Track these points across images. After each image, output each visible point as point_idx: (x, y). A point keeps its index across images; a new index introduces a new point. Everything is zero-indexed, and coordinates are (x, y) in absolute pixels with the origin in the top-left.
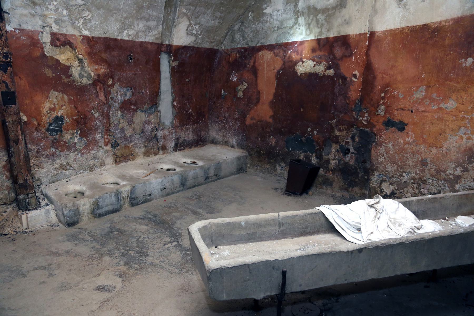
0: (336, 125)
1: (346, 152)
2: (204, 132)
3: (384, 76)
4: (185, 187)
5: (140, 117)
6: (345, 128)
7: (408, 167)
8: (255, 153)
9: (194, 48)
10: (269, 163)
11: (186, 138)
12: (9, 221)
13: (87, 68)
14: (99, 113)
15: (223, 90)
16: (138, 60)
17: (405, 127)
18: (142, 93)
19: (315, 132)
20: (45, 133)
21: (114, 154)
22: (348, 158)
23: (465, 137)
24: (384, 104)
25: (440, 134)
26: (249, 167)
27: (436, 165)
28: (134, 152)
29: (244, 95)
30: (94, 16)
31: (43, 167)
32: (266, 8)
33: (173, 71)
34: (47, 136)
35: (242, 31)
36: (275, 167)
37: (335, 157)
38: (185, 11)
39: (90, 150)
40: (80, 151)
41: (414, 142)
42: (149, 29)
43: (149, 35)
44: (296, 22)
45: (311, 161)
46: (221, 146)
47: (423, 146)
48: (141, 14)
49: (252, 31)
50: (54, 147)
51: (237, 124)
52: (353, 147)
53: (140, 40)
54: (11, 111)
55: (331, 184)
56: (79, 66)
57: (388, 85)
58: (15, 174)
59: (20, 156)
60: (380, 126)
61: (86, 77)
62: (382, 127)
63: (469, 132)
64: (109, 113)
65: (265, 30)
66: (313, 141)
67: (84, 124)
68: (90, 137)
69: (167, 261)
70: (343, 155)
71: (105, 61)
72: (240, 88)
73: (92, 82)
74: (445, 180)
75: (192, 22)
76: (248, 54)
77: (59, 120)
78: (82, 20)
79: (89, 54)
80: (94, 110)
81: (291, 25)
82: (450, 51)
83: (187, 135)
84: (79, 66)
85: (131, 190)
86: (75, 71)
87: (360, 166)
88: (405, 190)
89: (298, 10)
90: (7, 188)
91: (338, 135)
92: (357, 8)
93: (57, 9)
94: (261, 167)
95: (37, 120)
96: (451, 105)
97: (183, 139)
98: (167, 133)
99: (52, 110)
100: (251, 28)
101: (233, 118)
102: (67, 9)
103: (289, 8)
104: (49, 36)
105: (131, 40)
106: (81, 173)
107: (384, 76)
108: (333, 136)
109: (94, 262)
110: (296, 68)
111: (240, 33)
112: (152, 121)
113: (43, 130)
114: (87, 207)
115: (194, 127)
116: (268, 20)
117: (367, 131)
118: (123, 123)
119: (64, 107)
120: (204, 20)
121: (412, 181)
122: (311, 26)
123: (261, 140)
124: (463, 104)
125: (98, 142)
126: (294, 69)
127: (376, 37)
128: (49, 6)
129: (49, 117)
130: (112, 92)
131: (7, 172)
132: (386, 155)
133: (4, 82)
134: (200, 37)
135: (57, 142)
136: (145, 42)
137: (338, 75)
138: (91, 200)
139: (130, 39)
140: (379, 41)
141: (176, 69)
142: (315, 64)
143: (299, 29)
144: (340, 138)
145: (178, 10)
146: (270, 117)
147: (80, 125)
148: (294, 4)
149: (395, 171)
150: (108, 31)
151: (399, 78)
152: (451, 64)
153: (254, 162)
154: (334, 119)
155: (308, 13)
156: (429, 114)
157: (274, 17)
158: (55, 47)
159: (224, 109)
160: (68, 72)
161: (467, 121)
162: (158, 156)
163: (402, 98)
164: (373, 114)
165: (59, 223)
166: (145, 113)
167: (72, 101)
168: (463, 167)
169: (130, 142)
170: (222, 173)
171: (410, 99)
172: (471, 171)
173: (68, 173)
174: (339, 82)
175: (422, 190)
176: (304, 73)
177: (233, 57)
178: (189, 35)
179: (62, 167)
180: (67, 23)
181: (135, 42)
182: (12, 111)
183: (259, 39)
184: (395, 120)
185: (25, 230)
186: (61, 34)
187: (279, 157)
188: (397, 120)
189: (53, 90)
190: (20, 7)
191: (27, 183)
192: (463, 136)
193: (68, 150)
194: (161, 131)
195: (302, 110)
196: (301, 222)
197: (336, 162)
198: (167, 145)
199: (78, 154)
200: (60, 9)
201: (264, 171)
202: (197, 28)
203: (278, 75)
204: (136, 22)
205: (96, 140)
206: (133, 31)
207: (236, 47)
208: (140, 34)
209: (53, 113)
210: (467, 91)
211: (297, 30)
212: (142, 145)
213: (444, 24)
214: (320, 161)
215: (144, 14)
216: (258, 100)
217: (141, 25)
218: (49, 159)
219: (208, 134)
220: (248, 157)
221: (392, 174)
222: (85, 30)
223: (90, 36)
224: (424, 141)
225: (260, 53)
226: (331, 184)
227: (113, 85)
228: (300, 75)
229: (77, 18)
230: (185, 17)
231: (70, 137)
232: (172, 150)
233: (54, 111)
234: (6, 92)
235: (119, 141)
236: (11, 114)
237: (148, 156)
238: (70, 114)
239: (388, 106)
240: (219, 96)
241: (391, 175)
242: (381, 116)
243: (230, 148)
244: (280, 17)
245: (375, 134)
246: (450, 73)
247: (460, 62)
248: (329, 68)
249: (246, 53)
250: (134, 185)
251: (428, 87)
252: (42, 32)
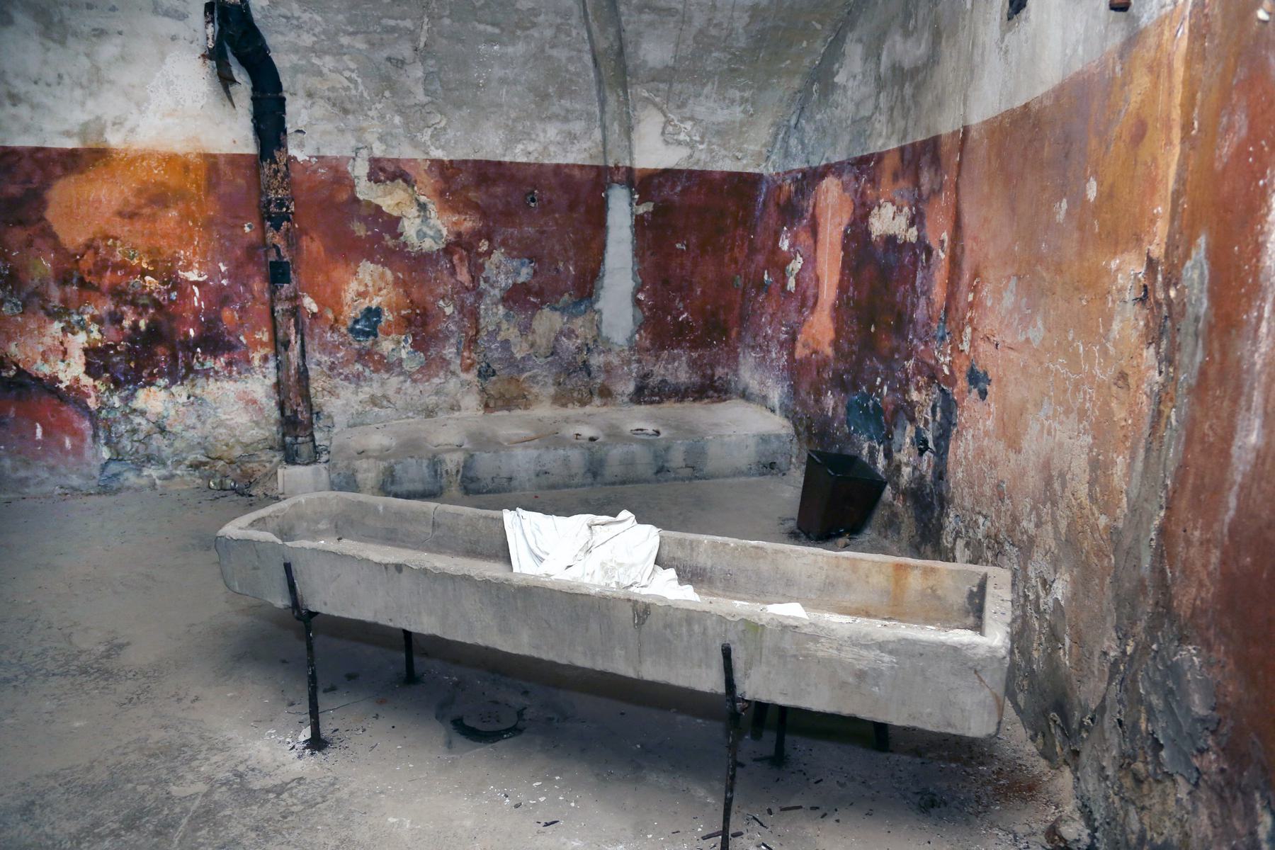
2: (723, 368)
4: (599, 478)
5: (548, 321)
9: (691, 173)
11: (670, 379)
16: (550, 202)
18: (557, 270)
21: (483, 390)
28: (530, 393)
31: (338, 395)
33: (639, 225)
38: (646, 94)
40: (410, 375)
42: (572, 137)
53: (555, 161)
56: (419, 216)
59: (288, 370)
61: (431, 237)
64: (478, 307)
68: (432, 352)
71: (476, 207)
73: (444, 246)
75: (672, 116)
77: (372, 314)
78: (429, 131)
79: (441, 194)
83: (670, 371)
84: (419, 216)
85: (465, 462)
86: (410, 228)
93: (382, 117)
95: (334, 311)
97: (660, 378)
98: (616, 361)
99: (362, 295)
102: (400, 112)
106: (408, 417)
112: (579, 331)
113: (343, 330)
114: (372, 475)
119: (384, 292)
120: (703, 109)
128: (369, 113)
129: (356, 308)
130: (486, 266)
133: (275, 246)
134: (701, 147)
136: (567, 166)
138: (381, 463)
139: (532, 159)
141: (647, 221)
150: (482, 147)
158: (376, 182)
162: (588, 409)
166: (562, 314)
169: (522, 371)
173: (383, 412)
180: (403, 139)
181: (542, 165)
186: (389, 160)
190: (322, 120)
193: (387, 371)
194: (599, 354)
196: (468, 529)
198: (613, 388)
199: (405, 381)
200: (388, 116)
202: (689, 128)
204: (539, 126)
205: (444, 359)
206: (537, 145)
215: (555, 109)
217: (552, 132)
220: (795, 440)
222: (437, 148)
227: (489, 253)
230: (650, 107)
232: (626, 399)
234: (276, 262)
235: (495, 366)
237: (564, 405)
252: (354, 159)
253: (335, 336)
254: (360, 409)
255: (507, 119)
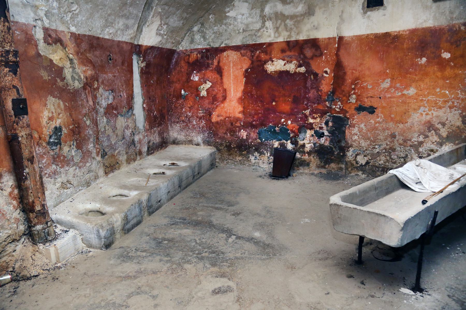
0: (310, 114)
1: (321, 135)
3: (354, 71)
5: (121, 121)
6: (319, 116)
7: (380, 140)
8: (224, 148)
9: (158, 48)
10: (241, 155)
12: (28, 260)
13: (77, 70)
14: (90, 120)
15: (183, 90)
17: (375, 110)
18: (121, 96)
19: (289, 122)
20: (46, 148)
22: (322, 140)
23: (424, 113)
24: (354, 93)
25: (405, 113)
26: (218, 162)
27: (403, 136)
29: (207, 94)
30: (82, 10)
32: (229, 12)
33: (143, 73)
34: (48, 151)
35: (202, 32)
36: (249, 157)
37: (310, 141)
39: (86, 163)
41: (383, 121)
42: (127, 27)
43: (126, 34)
44: (263, 26)
45: (286, 148)
46: (184, 145)
47: (391, 124)
48: (123, 11)
49: (214, 33)
50: (55, 163)
51: (202, 122)
52: (327, 131)
54: (23, 123)
55: (308, 165)
57: (357, 79)
58: (31, 200)
60: (352, 111)
62: (354, 112)
63: (427, 109)
65: (229, 32)
66: (288, 130)
67: (78, 134)
69: (246, 252)
70: (318, 139)
71: (90, 62)
72: (203, 88)
73: (82, 85)
74: (411, 146)
76: (211, 54)
77: (58, 130)
80: (86, 117)
81: (258, 28)
82: (408, 53)
85: (148, 198)
86: (68, 73)
87: (335, 146)
88: (378, 158)
89: (265, 15)
90: (16, 220)
91: (312, 122)
92: (325, 16)
94: (232, 160)
96: (412, 91)
97: (152, 142)
100: (213, 30)
101: (197, 117)
103: (254, 12)
104: (42, 31)
105: (110, 39)
106: (80, 190)
107: (354, 71)
108: (307, 123)
109: (180, 273)
110: (265, 66)
111: (200, 34)
113: (44, 144)
115: (159, 129)
116: (232, 23)
117: (340, 117)
118: (108, 129)
119: (61, 115)
121: (384, 151)
122: (280, 30)
123: (231, 135)
124: (421, 90)
125: (91, 153)
126: (264, 67)
127: (344, 41)
131: (14, 200)
132: (359, 134)
133: (14, 87)
134: (165, 37)
135: (57, 157)
136: (122, 42)
137: (309, 72)
140: (348, 44)
141: (144, 70)
142: (285, 63)
143: (267, 32)
144: (314, 125)
145: (154, 9)
146: (239, 113)
147: (75, 136)
148: (260, 9)
149: (368, 145)
151: (367, 73)
152: (410, 62)
153: (224, 156)
154: (308, 109)
155: (276, 18)
156: (394, 99)
157: (238, 20)
159: (185, 109)
160: (62, 75)
161: (425, 102)
162: (136, 162)
163: (370, 89)
164: (346, 101)
165: (88, 249)
167: (67, 108)
168: (425, 135)
169: (115, 150)
170: (202, 171)
171: (377, 89)
172: (430, 137)
173: (69, 191)
174: (311, 78)
175: (392, 157)
176: (275, 71)
177: (193, 57)
178: (158, 35)
179: (64, 186)
180: (57, 17)
181: (113, 41)
182: (25, 122)
183: (222, 41)
184: (366, 105)
185: (56, 265)
186: (52, 30)
187: (252, 149)
188: (368, 105)
189: (50, 95)
191: (45, 208)
192: (423, 113)
193: (67, 166)
195: (274, 103)
197: (311, 146)
199: (76, 169)
201: (236, 163)
203: (246, 73)
205: (89, 151)
206: (114, 29)
207: (196, 47)
208: (119, 32)
209: (51, 123)
210: (423, 81)
211: (265, 32)
212: (124, 153)
213: (402, 33)
214: (296, 146)
216: (225, 98)
217: (120, 23)
218: (51, 179)
219: (169, 135)
220: (217, 153)
221: (366, 147)
222: (73, 26)
223: (76, 33)
224: (392, 119)
225: (225, 54)
226: (308, 165)
227: (98, 88)
228: (270, 73)
229: (66, 11)
231: (68, 149)
232: (146, 154)
233: (52, 121)
234: (17, 99)
236: (23, 127)
238: (66, 123)
239: (359, 95)
240: (180, 96)
241: (365, 149)
242: (353, 103)
243: (195, 146)
244: (245, 21)
245: (348, 119)
246: (410, 69)
247: (416, 60)
248: (300, 66)
249: (208, 54)
250: (150, 193)
251: (392, 79)
253: (40, 149)
254: (58, 193)
255: (106, 14)
